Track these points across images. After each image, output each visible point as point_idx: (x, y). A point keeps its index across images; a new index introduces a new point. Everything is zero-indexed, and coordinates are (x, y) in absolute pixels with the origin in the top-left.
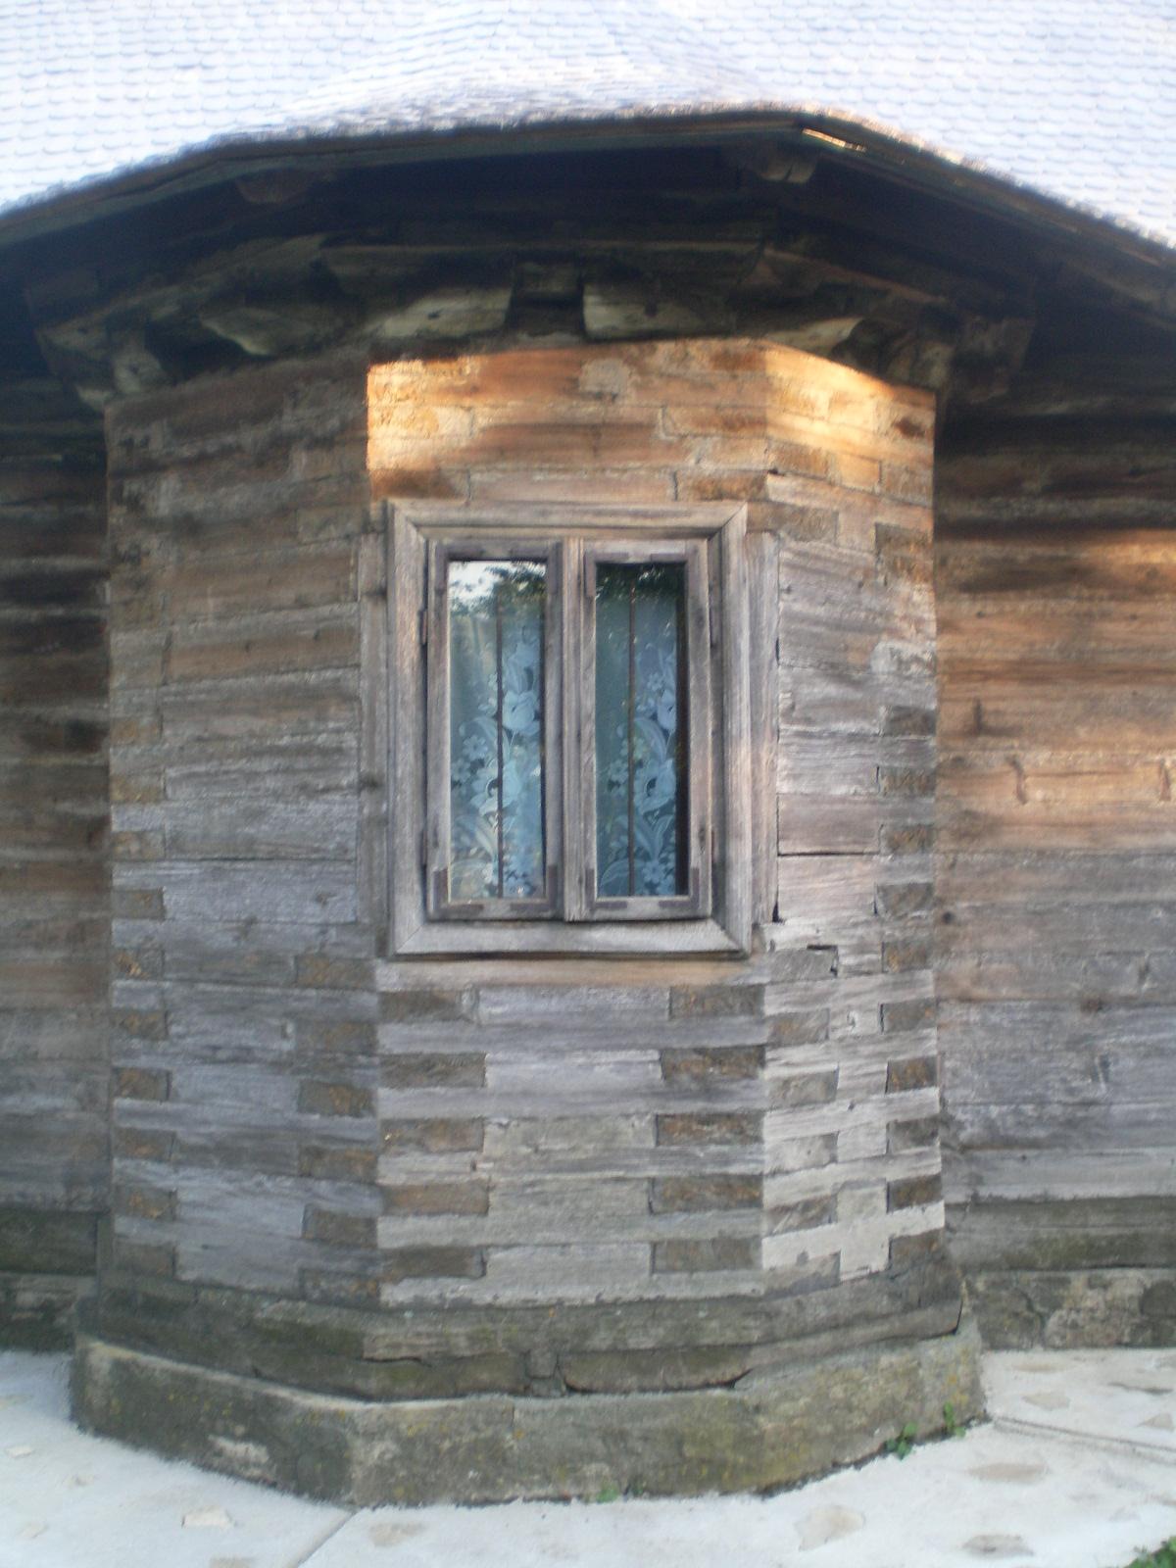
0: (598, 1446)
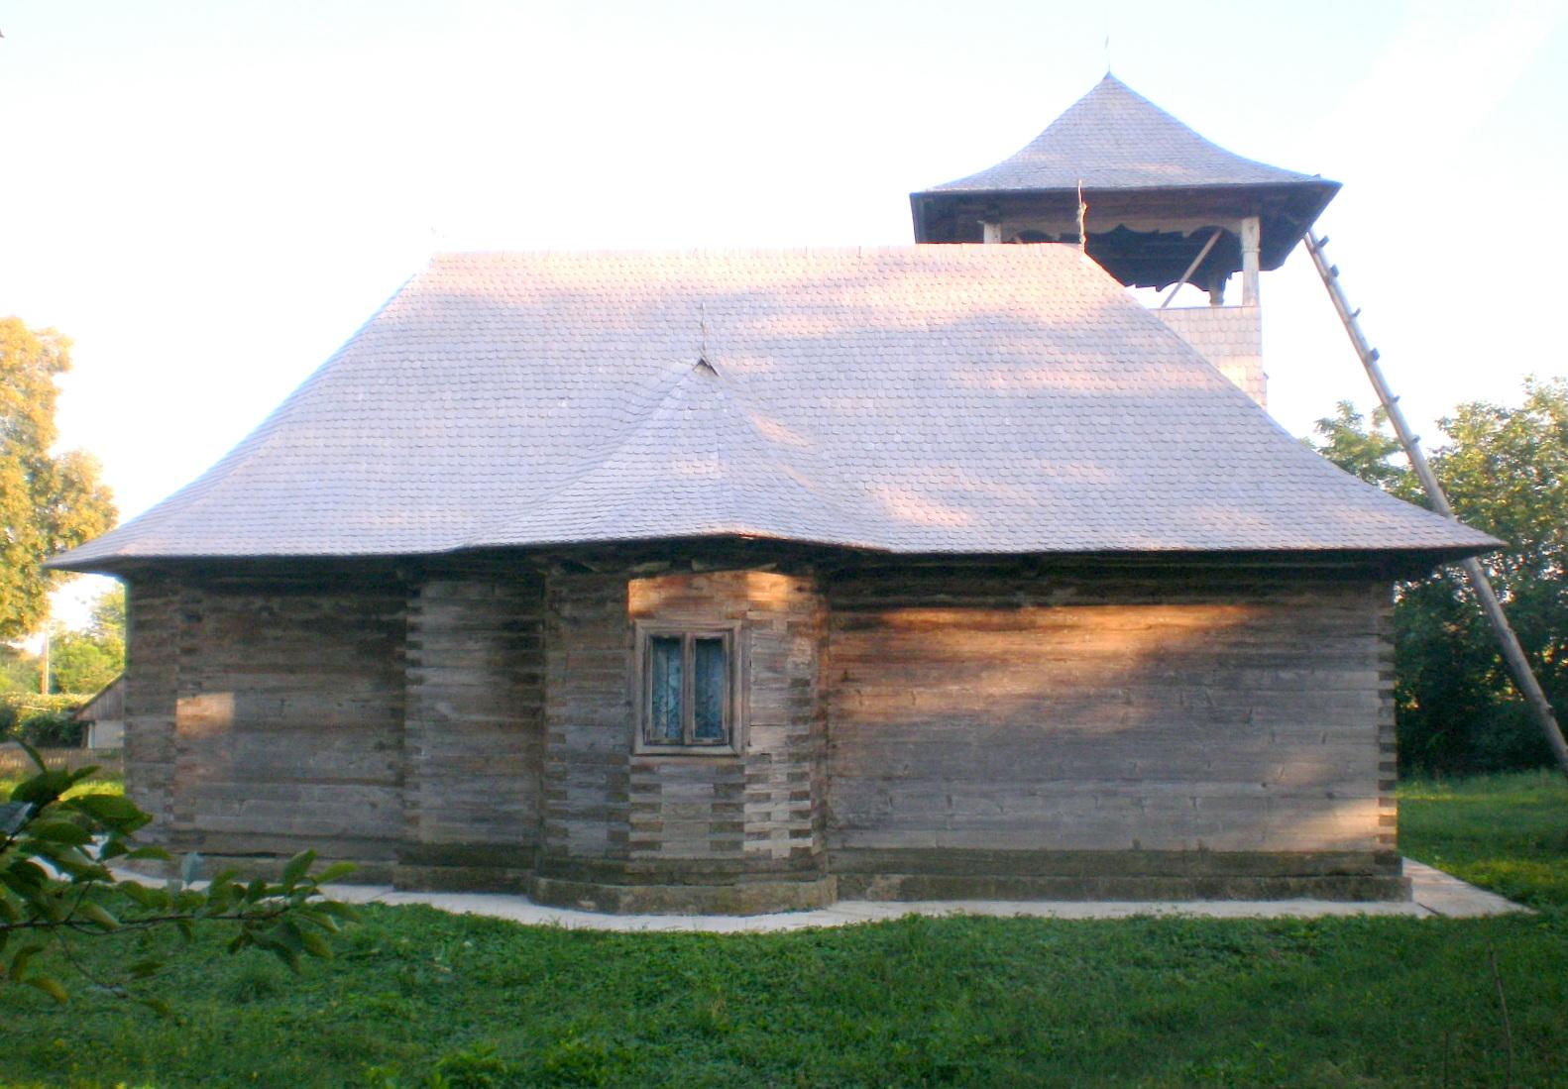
0: (692, 900)
